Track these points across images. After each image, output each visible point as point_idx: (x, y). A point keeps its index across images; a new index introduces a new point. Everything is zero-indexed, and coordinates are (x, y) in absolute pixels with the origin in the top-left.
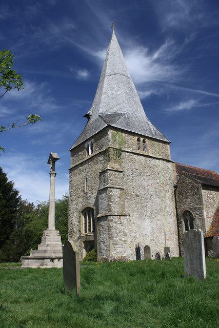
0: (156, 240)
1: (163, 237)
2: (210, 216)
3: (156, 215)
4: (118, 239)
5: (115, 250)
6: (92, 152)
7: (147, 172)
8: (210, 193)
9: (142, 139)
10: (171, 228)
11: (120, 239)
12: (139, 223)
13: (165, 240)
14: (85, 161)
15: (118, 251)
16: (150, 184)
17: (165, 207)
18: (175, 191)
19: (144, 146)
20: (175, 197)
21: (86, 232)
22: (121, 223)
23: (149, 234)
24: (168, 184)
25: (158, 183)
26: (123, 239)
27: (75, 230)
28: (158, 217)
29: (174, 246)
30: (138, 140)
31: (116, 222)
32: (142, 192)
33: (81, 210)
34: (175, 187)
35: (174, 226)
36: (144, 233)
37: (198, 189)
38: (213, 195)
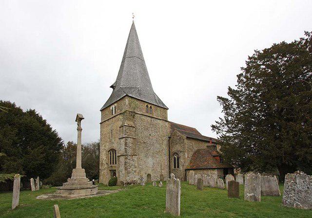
9: (149, 106)
18: (169, 140)
21: (111, 164)
31: (129, 160)
34: (170, 138)
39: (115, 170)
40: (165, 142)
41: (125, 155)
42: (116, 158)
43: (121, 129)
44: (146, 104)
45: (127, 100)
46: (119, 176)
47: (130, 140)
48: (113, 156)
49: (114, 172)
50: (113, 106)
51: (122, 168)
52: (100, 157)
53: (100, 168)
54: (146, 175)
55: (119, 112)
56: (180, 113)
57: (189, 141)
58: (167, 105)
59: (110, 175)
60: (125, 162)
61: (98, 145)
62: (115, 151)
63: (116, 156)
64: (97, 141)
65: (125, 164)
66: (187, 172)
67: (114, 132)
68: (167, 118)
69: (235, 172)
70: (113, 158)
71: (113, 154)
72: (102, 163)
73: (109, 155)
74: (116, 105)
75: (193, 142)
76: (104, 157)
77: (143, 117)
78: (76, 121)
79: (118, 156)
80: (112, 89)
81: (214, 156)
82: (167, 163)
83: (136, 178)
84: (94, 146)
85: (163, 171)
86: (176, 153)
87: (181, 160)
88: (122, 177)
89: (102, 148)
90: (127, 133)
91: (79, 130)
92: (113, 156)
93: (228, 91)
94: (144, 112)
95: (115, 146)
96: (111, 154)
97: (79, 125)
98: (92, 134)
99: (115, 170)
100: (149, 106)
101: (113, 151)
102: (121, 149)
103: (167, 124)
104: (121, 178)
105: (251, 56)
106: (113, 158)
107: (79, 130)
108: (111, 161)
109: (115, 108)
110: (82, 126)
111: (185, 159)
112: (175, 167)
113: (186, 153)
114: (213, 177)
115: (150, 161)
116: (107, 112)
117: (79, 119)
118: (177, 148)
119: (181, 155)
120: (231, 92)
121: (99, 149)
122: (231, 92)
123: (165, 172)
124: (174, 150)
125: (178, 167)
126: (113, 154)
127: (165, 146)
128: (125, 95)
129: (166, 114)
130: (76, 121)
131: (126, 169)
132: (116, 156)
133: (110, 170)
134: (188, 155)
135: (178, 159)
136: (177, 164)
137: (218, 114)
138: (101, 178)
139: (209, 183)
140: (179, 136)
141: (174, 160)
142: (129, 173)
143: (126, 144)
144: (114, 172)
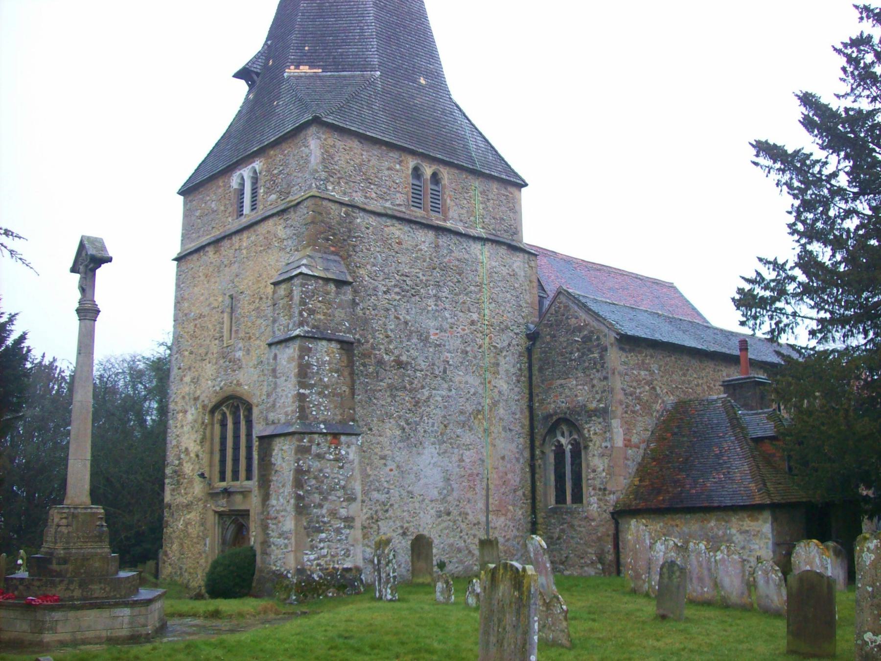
0: (455, 512)
1: (481, 505)
2: (635, 439)
3: (459, 431)
4: (324, 511)
5: (312, 548)
6: (254, 207)
7: (437, 285)
8: (642, 366)
9: (428, 171)
10: (509, 476)
11: (333, 514)
12: (401, 456)
13: (488, 511)
14: (249, 155)
15: (325, 551)
16: (446, 326)
17: (495, 404)
18: (529, 351)
19: (436, 196)
20: (530, 368)
21: (223, 478)
22: (336, 460)
23: (435, 493)
24: (507, 328)
25: (473, 323)
26: (343, 512)
27: (188, 468)
28: (467, 438)
29: (515, 532)
30: (417, 173)
31: (320, 457)
32: (412, 352)
33: (210, 406)
34: (533, 337)
35: (518, 467)
36: (416, 490)
37: (605, 349)
38: (652, 373)
39: (246, 514)
40: (509, 363)
41: (304, 432)
42: (249, 448)
43: (282, 290)
44: (412, 162)
45: (314, 145)
46: (266, 543)
47: (325, 354)
48: (237, 437)
49: (236, 523)
50: (246, 172)
51: (282, 499)
52: (172, 441)
53: (168, 498)
54: (407, 543)
55: (271, 201)
56: (571, 217)
57: (633, 359)
58: (518, 161)
59: (217, 539)
60: (299, 471)
61: (160, 369)
62: (249, 408)
63: (249, 435)
64: (163, 352)
65: (298, 483)
66: (623, 526)
67: (245, 307)
68: (516, 231)
69: (168, 579)
70: (236, 448)
71: (236, 423)
72: (178, 473)
73: (217, 428)
74: (258, 165)
75: (655, 363)
76: (187, 439)
77: (396, 231)
78: (74, 270)
79: (261, 438)
80: (242, 87)
81: (758, 440)
82: (517, 475)
83: (357, 556)
84: (136, 375)
85: (499, 522)
86: (567, 421)
87: (596, 463)
88: (284, 550)
89: (180, 390)
90: (312, 312)
91: (88, 312)
92: (237, 437)
93: (799, 111)
94: (399, 201)
95: (249, 381)
96: (223, 425)
97: (87, 288)
98: (138, 322)
99: (246, 514)
100: (428, 171)
101: (232, 407)
102: (277, 399)
103: (518, 262)
104: (276, 553)
105: (755, 153)
106: (236, 448)
107: (88, 312)
108: (223, 461)
109: (255, 180)
110: (100, 297)
111: (614, 456)
112: (560, 498)
113: (616, 423)
114: (742, 554)
115: (429, 467)
116: (212, 199)
117: (89, 260)
118: (575, 391)
119: (592, 429)
120: (819, 117)
121: (161, 391)
122: (819, 117)
123: (505, 526)
124: (556, 402)
125: (578, 497)
126: (236, 423)
127: (505, 384)
128: (308, 117)
129: (514, 209)
130: (74, 270)
131: (301, 508)
132: (249, 435)
133: (221, 514)
134: (628, 432)
135: (578, 451)
136: (570, 480)
137: (761, 229)
138: (172, 549)
139: (716, 585)
140: (580, 329)
141: (553, 442)
142: (319, 531)
143: (303, 373)
144: (236, 523)
